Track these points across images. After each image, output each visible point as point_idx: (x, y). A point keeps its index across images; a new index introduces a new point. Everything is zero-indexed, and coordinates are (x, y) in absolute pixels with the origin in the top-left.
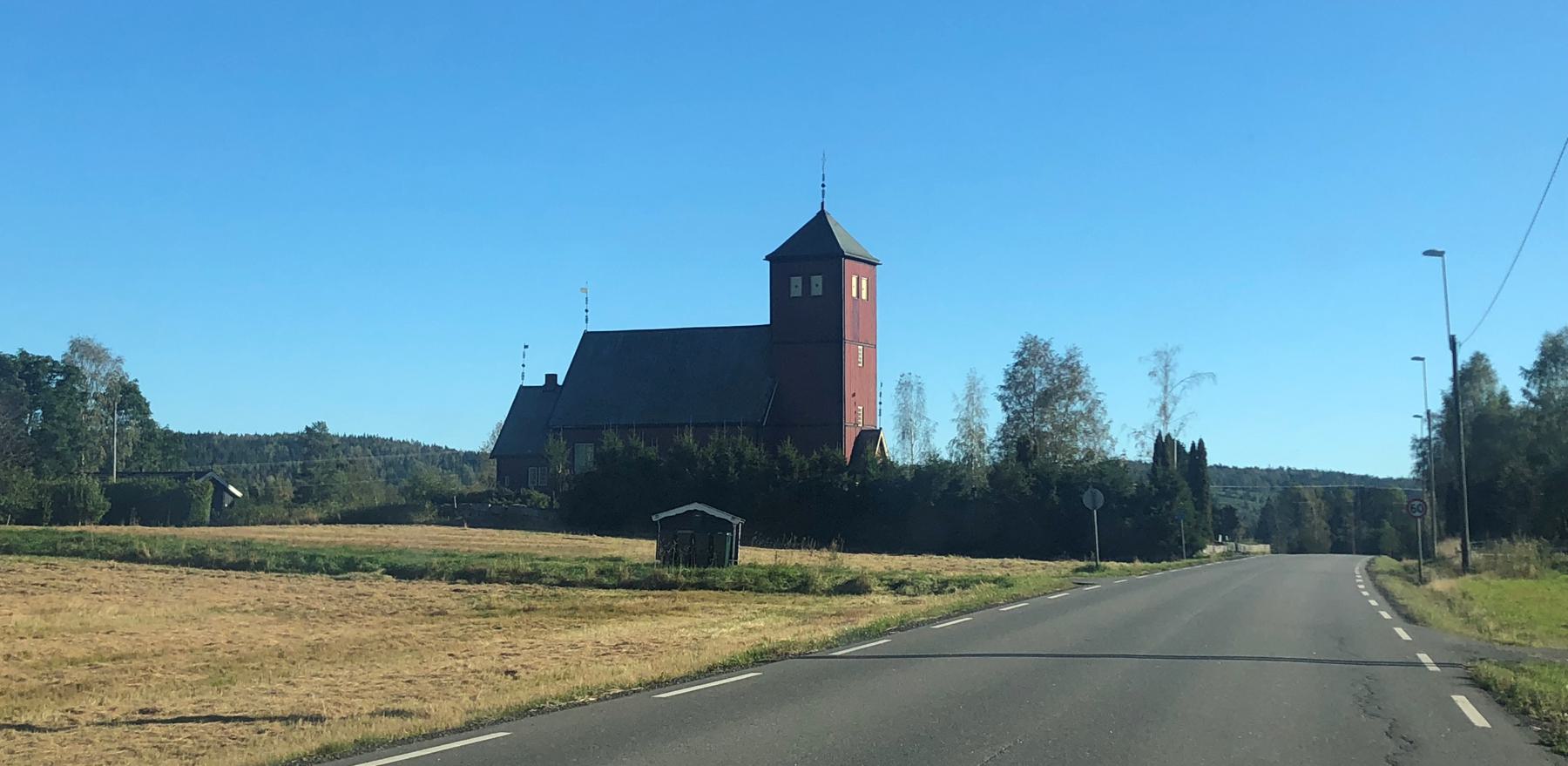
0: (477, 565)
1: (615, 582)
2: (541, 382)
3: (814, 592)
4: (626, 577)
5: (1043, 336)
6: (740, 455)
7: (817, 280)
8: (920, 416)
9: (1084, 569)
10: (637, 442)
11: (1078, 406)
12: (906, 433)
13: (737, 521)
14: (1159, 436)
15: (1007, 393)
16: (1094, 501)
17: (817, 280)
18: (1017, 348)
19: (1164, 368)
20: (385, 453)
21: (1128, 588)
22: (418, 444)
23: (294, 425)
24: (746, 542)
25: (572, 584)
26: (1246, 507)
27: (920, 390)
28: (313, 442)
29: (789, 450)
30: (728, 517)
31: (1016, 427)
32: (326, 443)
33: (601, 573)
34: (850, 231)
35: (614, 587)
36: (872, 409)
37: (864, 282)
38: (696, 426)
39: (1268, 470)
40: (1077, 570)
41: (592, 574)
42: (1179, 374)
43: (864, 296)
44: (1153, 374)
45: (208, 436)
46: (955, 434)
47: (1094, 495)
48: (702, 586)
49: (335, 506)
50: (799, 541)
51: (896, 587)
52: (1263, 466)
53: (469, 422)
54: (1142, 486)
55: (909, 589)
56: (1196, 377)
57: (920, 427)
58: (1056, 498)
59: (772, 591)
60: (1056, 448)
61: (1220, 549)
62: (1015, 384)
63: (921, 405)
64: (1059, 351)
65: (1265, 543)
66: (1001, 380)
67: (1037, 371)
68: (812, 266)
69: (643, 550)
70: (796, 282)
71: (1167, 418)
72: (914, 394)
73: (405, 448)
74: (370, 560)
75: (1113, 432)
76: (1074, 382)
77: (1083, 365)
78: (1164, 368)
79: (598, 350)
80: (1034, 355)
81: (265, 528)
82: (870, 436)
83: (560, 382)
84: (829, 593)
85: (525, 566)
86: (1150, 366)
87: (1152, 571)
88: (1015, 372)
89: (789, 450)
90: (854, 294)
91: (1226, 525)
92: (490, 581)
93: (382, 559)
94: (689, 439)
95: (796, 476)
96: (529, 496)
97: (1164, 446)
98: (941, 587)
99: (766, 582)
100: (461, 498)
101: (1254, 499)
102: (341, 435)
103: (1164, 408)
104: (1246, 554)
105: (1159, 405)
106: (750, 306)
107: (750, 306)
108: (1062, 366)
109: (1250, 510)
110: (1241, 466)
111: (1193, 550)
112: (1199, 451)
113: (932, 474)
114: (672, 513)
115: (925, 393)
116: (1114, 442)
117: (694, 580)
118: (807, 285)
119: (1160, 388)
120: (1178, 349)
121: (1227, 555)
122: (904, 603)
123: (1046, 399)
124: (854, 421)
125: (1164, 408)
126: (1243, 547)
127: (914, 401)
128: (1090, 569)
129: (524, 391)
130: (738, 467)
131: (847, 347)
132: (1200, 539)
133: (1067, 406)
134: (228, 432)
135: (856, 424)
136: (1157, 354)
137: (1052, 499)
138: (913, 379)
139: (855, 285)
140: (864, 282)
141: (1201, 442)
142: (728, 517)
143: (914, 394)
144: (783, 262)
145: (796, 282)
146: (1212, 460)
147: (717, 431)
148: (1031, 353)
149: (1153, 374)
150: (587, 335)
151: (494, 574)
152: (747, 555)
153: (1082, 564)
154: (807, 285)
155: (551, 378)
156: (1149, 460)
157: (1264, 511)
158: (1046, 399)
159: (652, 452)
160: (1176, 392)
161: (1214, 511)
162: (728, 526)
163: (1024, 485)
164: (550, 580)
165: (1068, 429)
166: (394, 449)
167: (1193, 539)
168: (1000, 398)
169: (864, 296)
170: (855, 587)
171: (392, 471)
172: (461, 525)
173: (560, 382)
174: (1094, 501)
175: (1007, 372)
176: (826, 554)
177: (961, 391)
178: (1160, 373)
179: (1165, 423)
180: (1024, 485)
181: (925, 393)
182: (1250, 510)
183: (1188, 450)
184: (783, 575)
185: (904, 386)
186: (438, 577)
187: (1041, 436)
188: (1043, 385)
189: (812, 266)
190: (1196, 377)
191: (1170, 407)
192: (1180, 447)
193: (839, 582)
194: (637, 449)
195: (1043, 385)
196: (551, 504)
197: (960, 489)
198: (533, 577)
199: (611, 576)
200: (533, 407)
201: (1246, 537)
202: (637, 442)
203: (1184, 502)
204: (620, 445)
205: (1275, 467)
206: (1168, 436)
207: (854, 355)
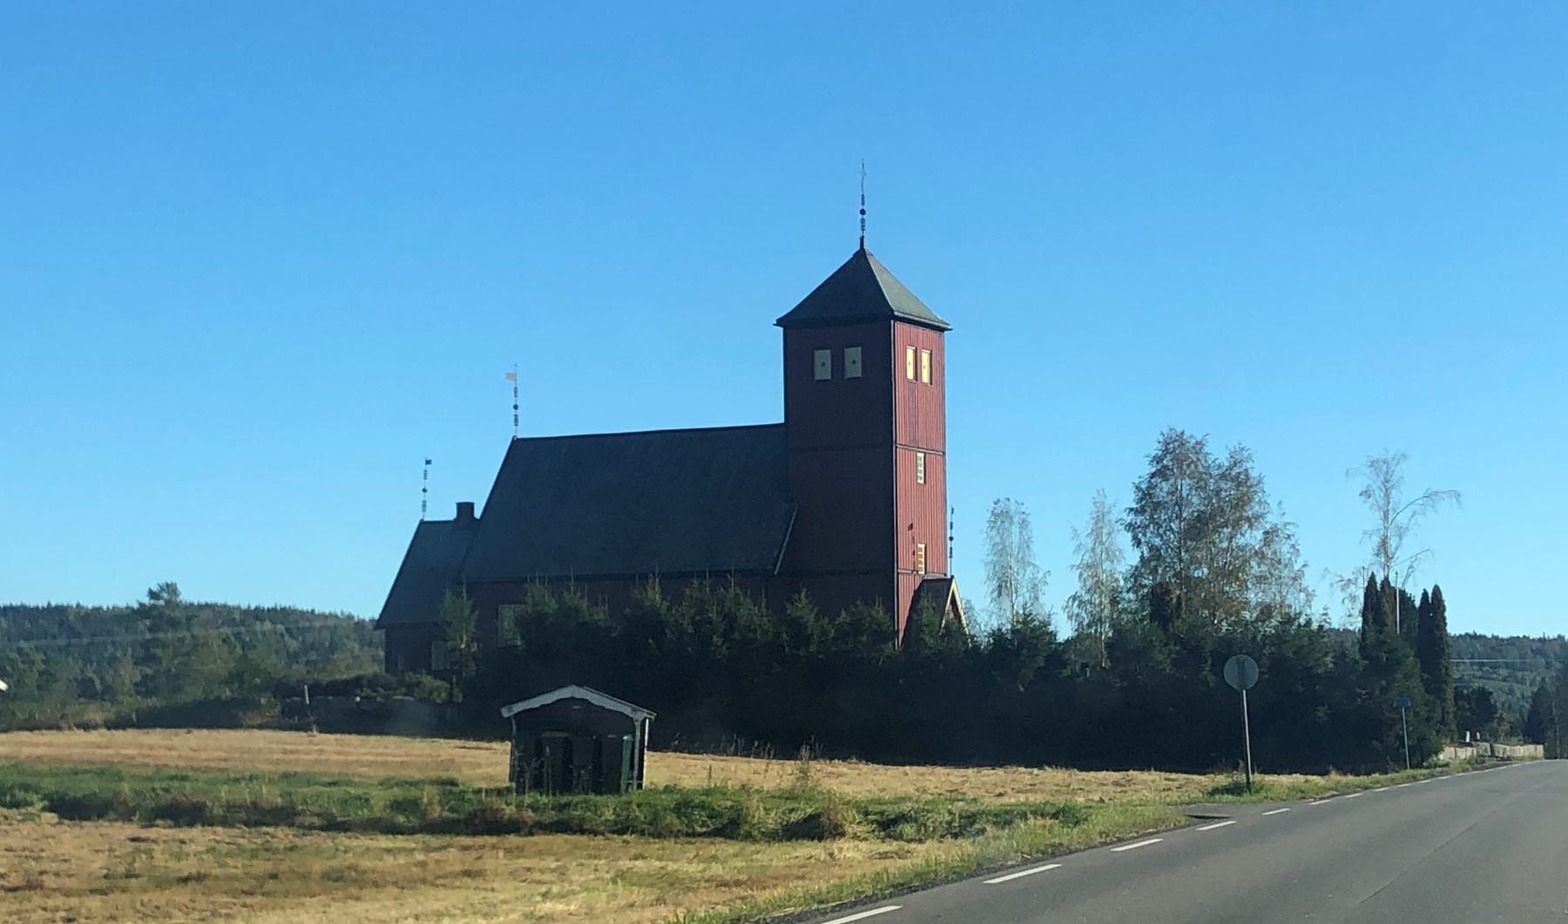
0: (188, 792)
1: (414, 821)
2: (450, 514)
3: (748, 837)
4: (436, 812)
5: (1193, 432)
6: (730, 619)
7: (854, 354)
8: (1024, 562)
9: (1227, 790)
10: (576, 599)
11: (1251, 538)
12: (1003, 587)
13: (641, 715)
14: (1372, 579)
15: (1139, 519)
16: (1242, 673)
17: (854, 354)
18: (1154, 449)
19: (1383, 482)
20: (303, 631)
21: (1304, 815)
22: (350, 617)
23: (121, 590)
24: (654, 747)
25: (343, 827)
26: (1511, 692)
27: (1024, 524)
28: (162, 616)
29: (803, 608)
30: (626, 709)
31: (1154, 571)
32: (177, 614)
33: (397, 806)
34: (901, 281)
35: (411, 831)
36: (941, 547)
37: (925, 357)
38: (665, 577)
39: (1542, 640)
40: (1215, 791)
41: (378, 808)
42: (1407, 492)
43: (925, 378)
44: (1366, 493)
45: (61, 610)
46: (1075, 587)
47: (1241, 664)
48: (562, 827)
49: (130, 703)
50: (749, 744)
51: (888, 824)
52: (1535, 634)
53: (347, 576)
54: (1344, 655)
55: (908, 829)
56: (1431, 497)
57: (1023, 579)
59: (677, 835)
60: (1212, 603)
61: (1465, 753)
63: (1026, 544)
64: (1218, 453)
65: (1537, 743)
66: (1131, 500)
67: (1185, 484)
68: (846, 331)
69: (487, 763)
70: (854, 370)
71: (1388, 558)
72: (1015, 529)
73: (331, 623)
74: (26, 788)
75: (1308, 581)
76: (1242, 502)
77: (1254, 474)
78: (1383, 482)
79: (529, 462)
80: (1179, 461)
81: (25, 736)
82: (937, 589)
83: (478, 514)
84: (773, 837)
85: (271, 796)
86: (1360, 484)
87: (1348, 789)
88: (1151, 487)
89: (803, 608)
90: (910, 375)
91: (1476, 716)
92: (209, 822)
93: (49, 785)
94: (653, 594)
95: (813, 648)
96: (418, 684)
97: (1379, 599)
98: (965, 825)
99: (671, 819)
100: (316, 689)
101: (1522, 682)
102: (244, 606)
103: (1384, 543)
104: (1508, 759)
105: (1376, 540)
106: (752, 395)
107: (752, 395)
108: (1223, 476)
109: (1511, 694)
110: (1504, 635)
111: (1421, 755)
112: (1434, 605)
113: (1025, 642)
114: (536, 703)
115: (1017, 524)
116: (1310, 597)
117: (551, 816)
118: (838, 364)
119: (1379, 515)
120: (1405, 456)
121: (1477, 763)
122: (884, 856)
123: (1199, 528)
124: (912, 565)
125: (1384, 543)
126: (1502, 749)
127: (1015, 539)
128: (1235, 790)
129: (426, 530)
130: (726, 636)
131: (901, 456)
133: (1231, 539)
134: (89, 603)
135: (915, 570)
136: (1372, 464)
137: (1204, 683)
138: (1013, 508)
139: (911, 362)
140: (925, 357)
141: (1437, 591)
142: (626, 709)
143: (1015, 529)
144: (805, 329)
145: (823, 357)
146: (1457, 624)
147: (696, 582)
148: (1176, 457)
149: (1366, 493)
150: (516, 444)
151: (218, 811)
152: (664, 770)
153: (1222, 780)
154: (838, 364)
155: (465, 508)
156: (1357, 623)
157: (1536, 696)
158: (1199, 528)
159: (601, 615)
160: (1402, 519)
161: (1458, 695)
162: (628, 725)
163: (1162, 657)
164: (308, 820)
165: (1232, 573)
166: (317, 624)
167: (1422, 739)
168: (1130, 527)
169: (925, 378)
170: (815, 828)
171: (313, 656)
172: (304, 728)
173: (478, 514)
174: (1242, 673)
175: (1138, 488)
176: (790, 766)
177: (1084, 524)
178: (1379, 494)
179: (1386, 566)
180: (1162, 657)
181: (1017, 524)
182: (1511, 694)
183: (1417, 604)
184: (702, 806)
185: (1000, 517)
186: (127, 817)
187: (1185, 580)
188: (1193, 505)
189: (846, 331)
190: (1431, 497)
191: (1393, 542)
192: (1405, 599)
193: (794, 817)
194: (577, 610)
195: (1193, 505)
196: (451, 695)
197: (1064, 665)
198: (284, 815)
199: (407, 815)
200: (437, 555)
201: (1511, 733)
202: (576, 599)
203: (1410, 682)
204: (554, 605)
205: (1552, 635)
206: (1386, 581)
207: (910, 468)
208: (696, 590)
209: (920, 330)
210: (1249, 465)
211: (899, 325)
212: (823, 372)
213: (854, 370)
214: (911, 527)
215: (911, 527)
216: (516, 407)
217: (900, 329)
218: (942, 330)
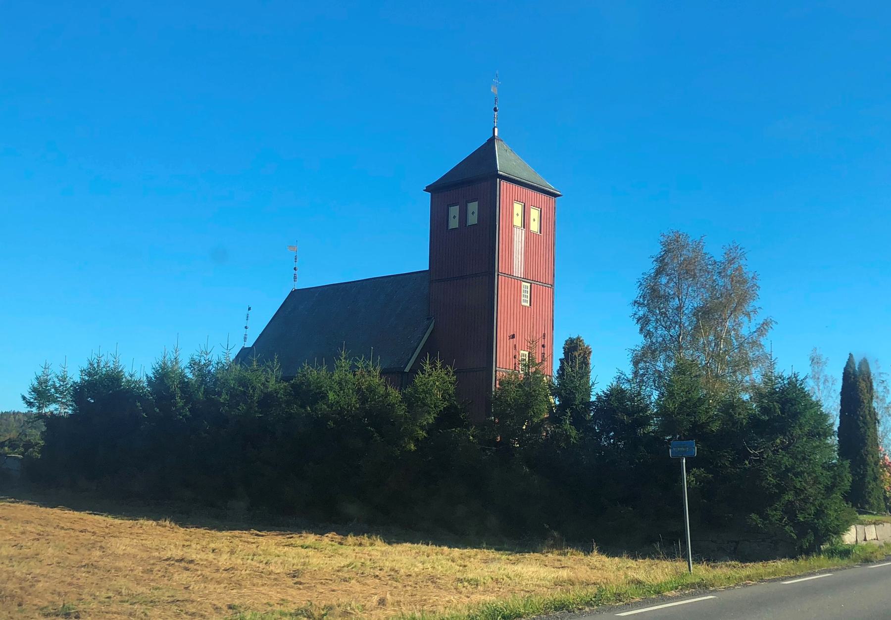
18: (658, 250)
37: (534, 214)
58: (574, 433)
62: (653, 298)
64: (715, 251)
132: (836, 506)
140: (534, 214)
145: (454, 211)
189: (468, 193)
195: (688, 294)
208: (370, 416)
209: (530, 192)
210: (743, 262)
211: (504, 185)
212: (454, 223)
213: (473, 219)
214: (513, 336)
215: (513, 336)
216: (295, 269)
217: (504, 187)
218: (556, 196)
